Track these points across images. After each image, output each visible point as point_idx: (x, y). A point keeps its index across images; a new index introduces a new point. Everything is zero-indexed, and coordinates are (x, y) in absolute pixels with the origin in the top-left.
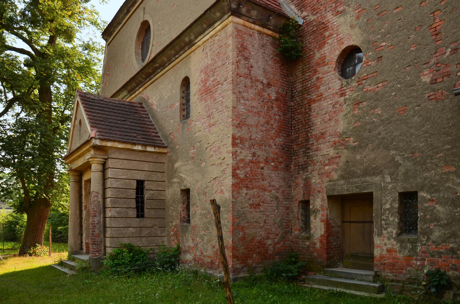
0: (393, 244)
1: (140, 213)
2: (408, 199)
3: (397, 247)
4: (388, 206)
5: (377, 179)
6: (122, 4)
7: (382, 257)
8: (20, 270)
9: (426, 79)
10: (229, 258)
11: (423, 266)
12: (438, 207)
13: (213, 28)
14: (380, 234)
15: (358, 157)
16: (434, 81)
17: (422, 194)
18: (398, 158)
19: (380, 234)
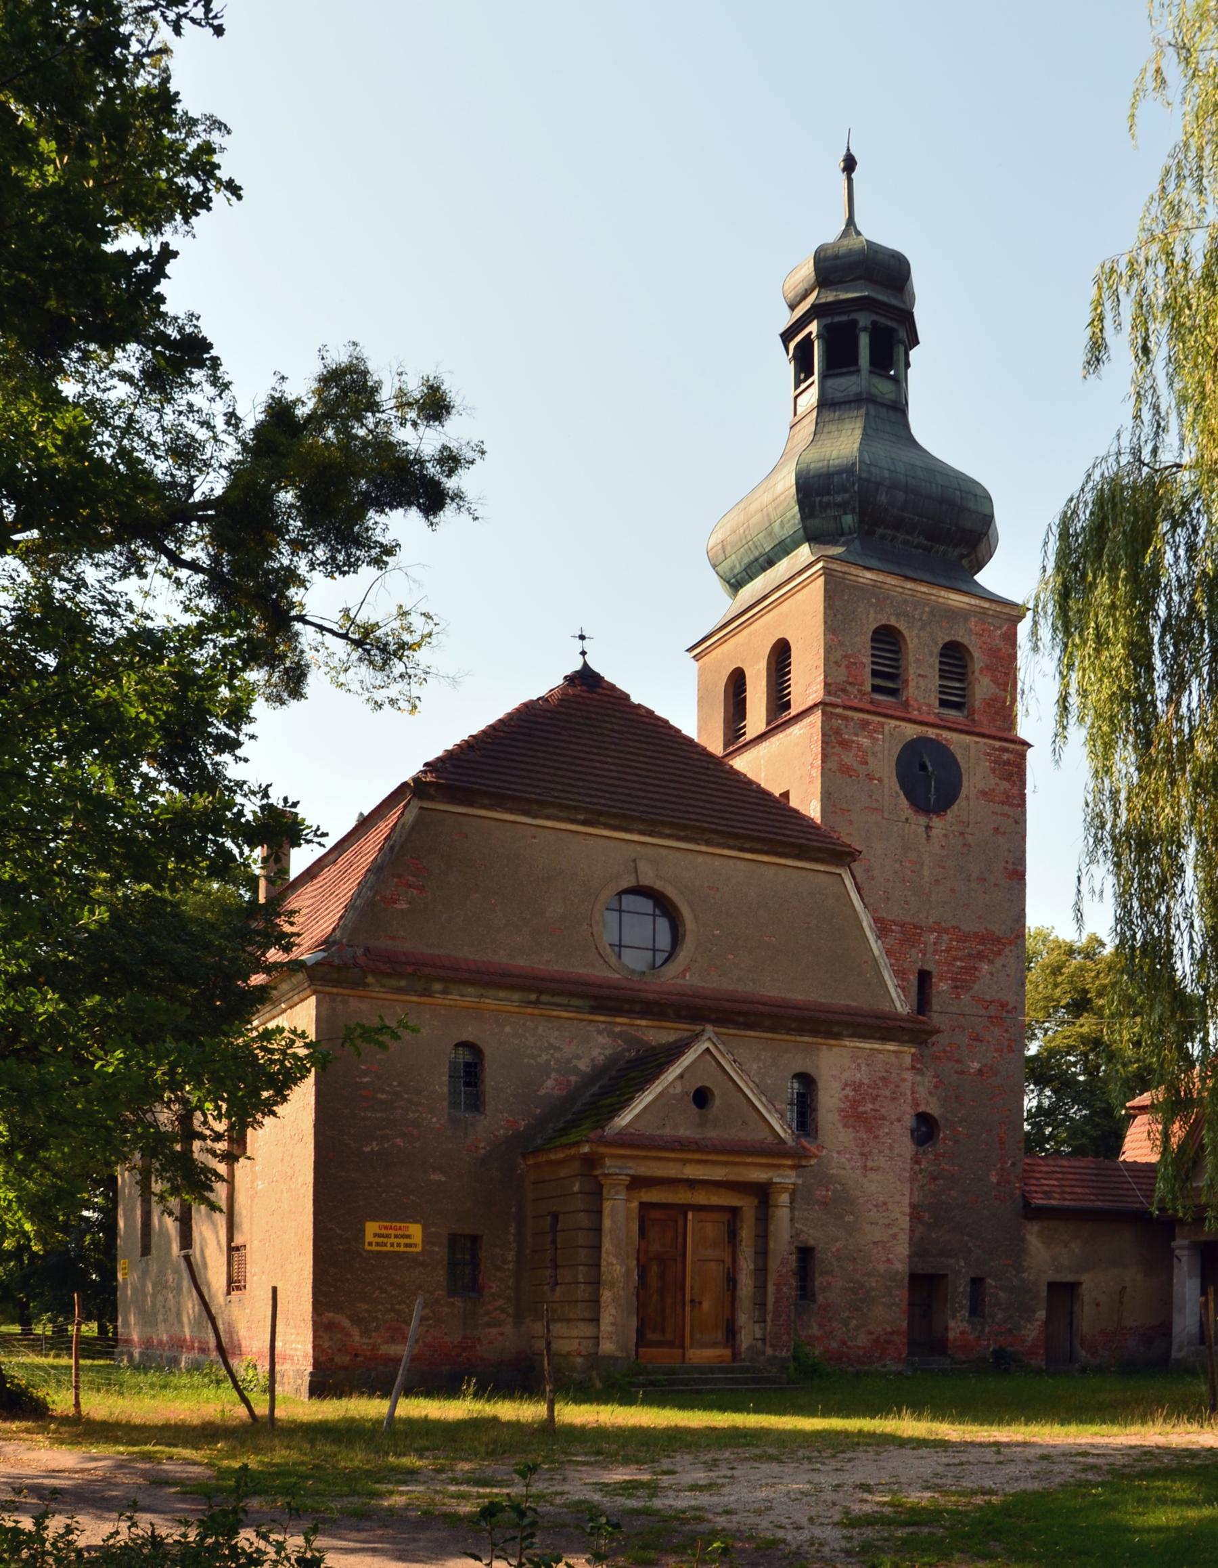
0: (965, 1326)
1: (275, 1290)
2: (977, 1282)
3: (969, 1329)
4: (961, 1289)
5: (952, 1261)
6: (377, 803)
7: (955, 1340)
8: (313, 1098)
9: (994, 1179)
10: (643, 1169)
11: (989, 1345)
12: (1001, 1293)
13: (934, 580)
14: (954, 1317)
15: (934, 1236)
16: (998, 1184)
17: (989, 1281)
18: (970, 1244)
19: (954, 1317)
